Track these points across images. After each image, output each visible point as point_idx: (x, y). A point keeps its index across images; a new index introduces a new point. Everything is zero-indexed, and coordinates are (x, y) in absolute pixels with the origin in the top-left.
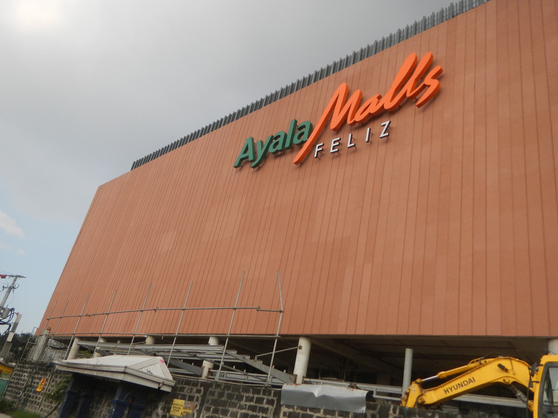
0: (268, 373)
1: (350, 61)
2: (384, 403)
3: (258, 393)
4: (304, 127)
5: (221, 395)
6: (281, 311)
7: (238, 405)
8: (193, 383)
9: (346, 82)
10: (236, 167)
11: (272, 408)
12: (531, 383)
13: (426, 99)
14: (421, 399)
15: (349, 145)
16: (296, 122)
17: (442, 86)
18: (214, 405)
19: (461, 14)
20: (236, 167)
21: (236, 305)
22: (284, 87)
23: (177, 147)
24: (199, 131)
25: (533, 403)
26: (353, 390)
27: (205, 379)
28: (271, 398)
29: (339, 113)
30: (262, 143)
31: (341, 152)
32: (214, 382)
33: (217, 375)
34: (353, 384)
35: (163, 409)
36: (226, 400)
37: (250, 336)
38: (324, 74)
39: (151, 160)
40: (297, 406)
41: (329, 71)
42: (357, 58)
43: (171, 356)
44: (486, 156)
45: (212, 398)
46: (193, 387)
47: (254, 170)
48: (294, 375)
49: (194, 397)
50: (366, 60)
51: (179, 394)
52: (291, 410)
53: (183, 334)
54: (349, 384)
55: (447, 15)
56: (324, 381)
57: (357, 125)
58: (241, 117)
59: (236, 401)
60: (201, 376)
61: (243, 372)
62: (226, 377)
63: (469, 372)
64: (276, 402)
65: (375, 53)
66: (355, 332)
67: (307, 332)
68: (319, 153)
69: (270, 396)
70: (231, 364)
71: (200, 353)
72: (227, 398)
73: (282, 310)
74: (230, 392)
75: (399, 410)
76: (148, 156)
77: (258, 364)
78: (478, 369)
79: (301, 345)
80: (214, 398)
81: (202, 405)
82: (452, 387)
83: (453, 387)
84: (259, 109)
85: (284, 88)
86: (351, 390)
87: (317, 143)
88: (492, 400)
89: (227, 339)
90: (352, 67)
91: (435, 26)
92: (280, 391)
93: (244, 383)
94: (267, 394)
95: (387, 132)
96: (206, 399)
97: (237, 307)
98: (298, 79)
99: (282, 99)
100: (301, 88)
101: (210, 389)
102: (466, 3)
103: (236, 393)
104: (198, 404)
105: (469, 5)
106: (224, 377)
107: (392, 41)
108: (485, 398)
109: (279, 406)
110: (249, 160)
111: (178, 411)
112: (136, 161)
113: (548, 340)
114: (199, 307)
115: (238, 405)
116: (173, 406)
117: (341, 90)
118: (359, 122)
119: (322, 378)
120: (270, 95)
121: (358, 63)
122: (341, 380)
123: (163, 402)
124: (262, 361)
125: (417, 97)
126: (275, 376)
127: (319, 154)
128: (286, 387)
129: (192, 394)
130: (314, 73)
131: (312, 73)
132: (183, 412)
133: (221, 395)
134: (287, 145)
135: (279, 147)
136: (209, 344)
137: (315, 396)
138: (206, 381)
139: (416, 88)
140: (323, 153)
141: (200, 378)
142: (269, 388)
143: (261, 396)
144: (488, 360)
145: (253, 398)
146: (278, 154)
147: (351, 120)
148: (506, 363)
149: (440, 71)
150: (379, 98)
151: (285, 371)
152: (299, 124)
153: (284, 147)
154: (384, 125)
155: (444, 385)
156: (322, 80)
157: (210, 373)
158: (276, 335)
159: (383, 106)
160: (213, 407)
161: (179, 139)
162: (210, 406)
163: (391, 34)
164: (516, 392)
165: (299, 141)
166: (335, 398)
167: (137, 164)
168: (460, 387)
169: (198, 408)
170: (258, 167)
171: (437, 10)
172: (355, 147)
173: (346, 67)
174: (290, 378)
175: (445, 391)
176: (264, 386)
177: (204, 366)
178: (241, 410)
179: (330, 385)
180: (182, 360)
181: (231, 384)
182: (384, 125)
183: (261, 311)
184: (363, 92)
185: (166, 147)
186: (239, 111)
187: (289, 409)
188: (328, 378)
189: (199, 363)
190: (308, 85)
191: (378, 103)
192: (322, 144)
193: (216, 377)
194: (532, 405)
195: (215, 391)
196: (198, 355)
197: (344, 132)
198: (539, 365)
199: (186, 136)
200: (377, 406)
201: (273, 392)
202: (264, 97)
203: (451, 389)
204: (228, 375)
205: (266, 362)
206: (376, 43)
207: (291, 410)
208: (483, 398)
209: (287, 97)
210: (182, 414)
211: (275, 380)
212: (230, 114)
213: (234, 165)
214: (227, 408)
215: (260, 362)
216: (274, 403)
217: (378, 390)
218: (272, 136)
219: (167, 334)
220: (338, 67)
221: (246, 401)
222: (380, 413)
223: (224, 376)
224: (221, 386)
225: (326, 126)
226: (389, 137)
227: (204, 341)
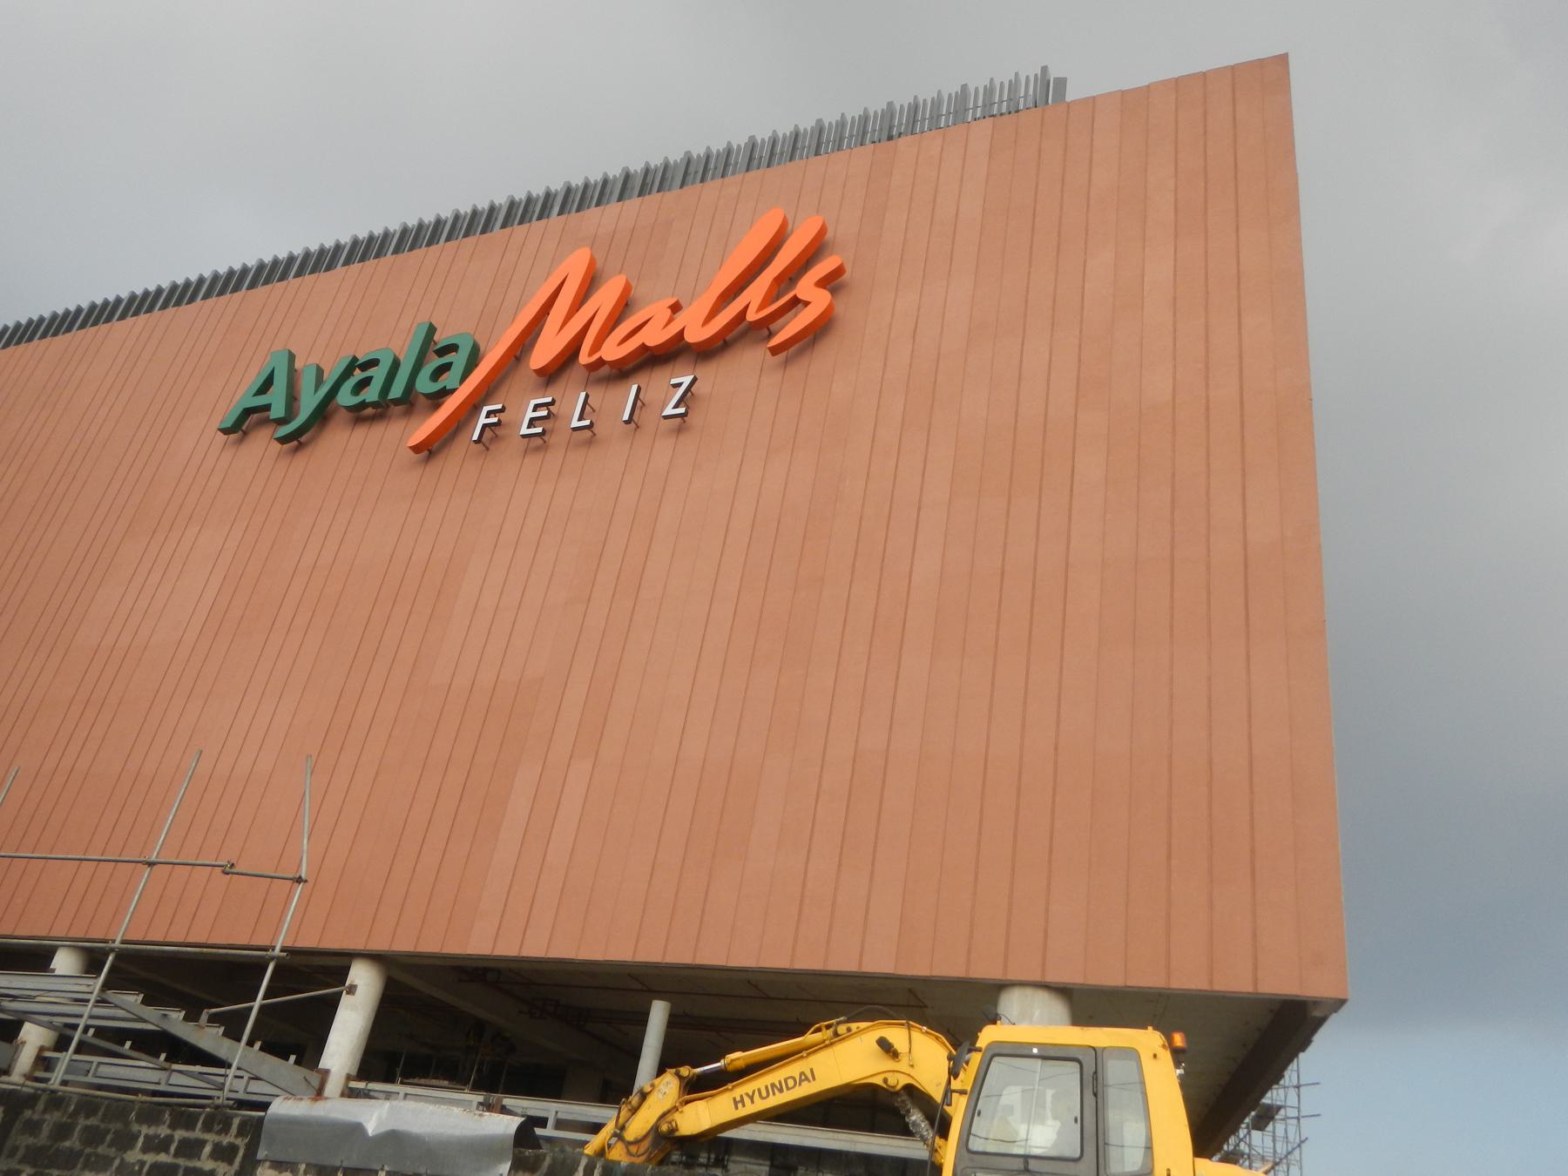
0: (230, 1060)
1: (611, 193)
2: (563, 1151)
3: (190, 1125)
4: (453, 348)
5: (62, 1131)
6: (300, 877)
7: (117, 1162)
9: (591, 249)
10: (226, 431)
12: (948, 1092)
14: (670, 1123)
15: (575, 423)
16: (432, 330)
17: (839, 309)
19: (910, 138)
20: (226, 431)
21: (158, 854)
25: (946, 1145)
26: (480, 1115)
27: (21, 1080)
28: (226, 1140)
29: (559, 331)
30: (320, 372)
31: (552, 439)
32: (44, 1090)
33: (57, 1070)
34: (494, 1097)
37: (189, 949)
38: (534, 212)
40: (307, 1165)
41: (549, 205)
42: (632, 189)
44: (919, 509)
45: (31, 1141)
47: (281, 449)
48: (319, 1071)
50: (653, 198)
54: (481, 1099)
55: (875, 131)
56: (409, 1090)
57: (605, 370)
58: (266, 282)
59: (112, 1152)
61: (155, 1060)
62: (95, 1076)
63: (804, 1054)
65: (681, 187)
67: (380, 944)
68: (487, 429)
69: (226, 1134)
70: (119, 1035)
71: (14, 998)
72: (80, 1141)
73: (303, 876)
74: (93, 1121)
75: (601, 1169)
77: (208, 1037)
78: (826, 1046)
79: (355, 984)
80: (35, 1141)
82: (754, 1092)
83: (757, 1092)
84: (325, 271)
86: (476, 1116)
87: (485, 402)
88: (851, 1141)
90: (613, 208)
91: (842, 150)
92: (261, 1120)
93: (155, 1093)
94: (217, 1128)
95: (683, 404)
97: (159, 860)
99: (401, 256)
100: (248, 289)
101: (28, 1113)
102: (900, 119)
103: (116, 1126)
105: (931, 117)
106: (87, 1075)
107: (755, 159)
108: (836, 1136)
110: (271, 417)
113: (1000, 987)
114: (33, 853)
115: (117, 1162)
117: (574, 267)
118: (612, 364)
121: (632, 200)
122: (460, 1087)
124: (223, 1028)
125: (773, 327)
126: (258, 1075)
127: (488, 433)
128: (281, 1107)
130: (620, 175)
131: (501, 200)
133: (62, 1131)
134: (396, 391)
135: (371, 394)
136: (53, 970)
137: (368, 1135)
138: (19, 1088)
139: (773, 302)
140: (499, 431)
142: (228, 1111)
143: (197, 1134)
144: (854, 1026)
145: (170, 1139)
146: (361, 415)
147: (590, 355)
148: (896, 1035)
149: (839, 271)
150: (676, 308)
151: (293, 1058)
152: (441, 339)
155: (734, 1087)
156: (526, 226)
157: (43, 1062)
158: (273, 950)
159: (682, 332)
161: (85, 305)
162: (18, 1167)
163: (729, 143)
164: (908, 1111)
165: (434, 387)
166: (427, 1139)
168: (774, 1094)
170: (296, 440)
171: (853, 112)
172: (592, 432)
173: (598, 205)
174: (306, 1080)
175: (736, 1103)
176: (212, 1103)
177: (24, 1039)
179: (416, 1101)
180: (91, 1031)
181: (102, 1097)
182: (679, 385)
183: (237, 874)
184: (633, 284)
186: (405, 231)
188: (423, 1081)
190: (484, 232)
191: (670, 321)
192: (499, 407)
193: (55, 1074)
194: (940, 1147)
195: (45, 1121)
197: (566, 384)
198: (973, 1049)
199: (111, 299)
200: (544, 1159)
201: (236, 1122)
203: (752, 1098)
204: (104, 1070)
205: (234, 1034)
206: (689, 161)
208: (830, 1135)
209: (416, 252)
211: (255, 1087)
213: (221, 422)
215: (216, 1029)
216: (235, 1156)
217: (560, 1116)
218: (355, 359)
220: (577, 199)
221: (145, 1150)
223: (89, 1071)
224: (68, 1105)
225: (518, 359)
226: (685, 418)
227: (35, 958)
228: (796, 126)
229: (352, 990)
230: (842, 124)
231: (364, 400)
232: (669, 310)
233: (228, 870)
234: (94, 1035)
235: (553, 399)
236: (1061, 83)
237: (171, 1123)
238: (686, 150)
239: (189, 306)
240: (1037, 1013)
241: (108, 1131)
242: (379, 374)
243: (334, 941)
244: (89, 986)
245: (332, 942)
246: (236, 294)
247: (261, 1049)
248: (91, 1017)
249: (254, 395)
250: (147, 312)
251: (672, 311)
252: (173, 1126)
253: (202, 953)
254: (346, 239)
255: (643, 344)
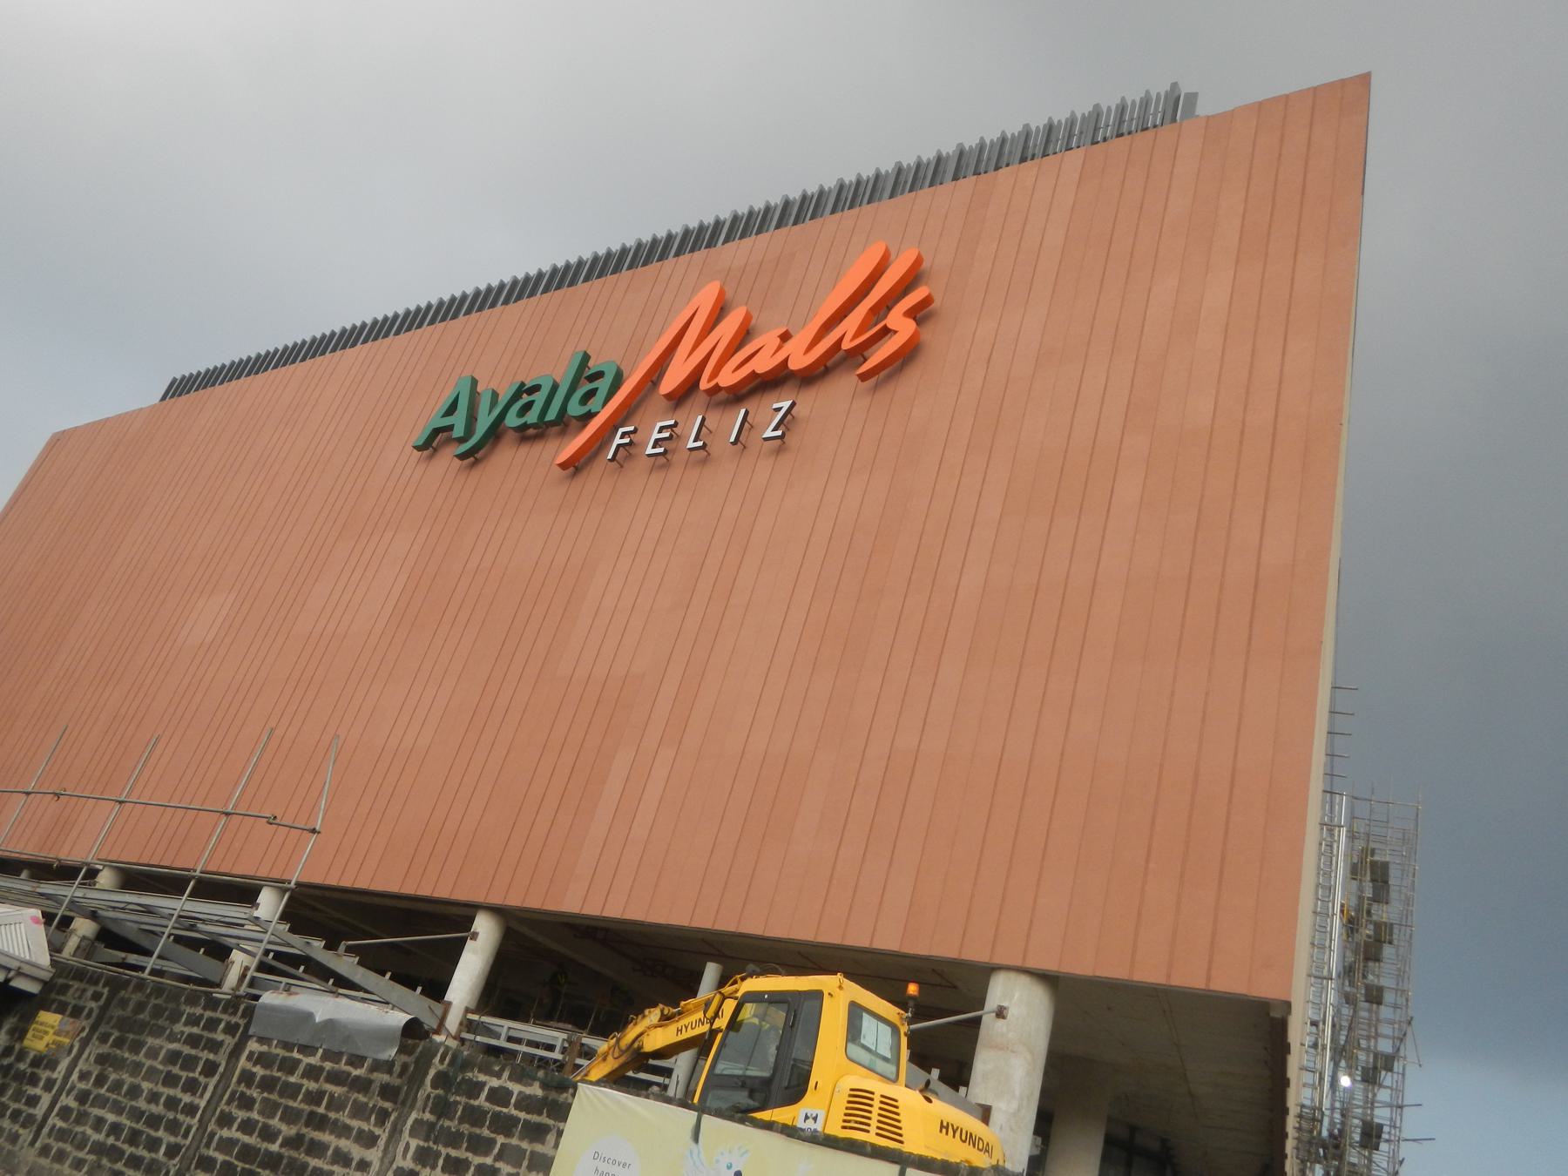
3: (214, 1009)
5: (140, 1007)
6: (314, 829)
8: (91, 978)
10: (418, 448)
11: (230, 1041)
13: (882, 362)
15: (691, 444)
16: (586, 358)
18: (120, 1030)
20: (418, 448)
22: (646, 238)
23: (242, 375)
24: (396, 316)
27: (67, 957)
28: (234, 1020)
30: (495, 395)
35: (11, 1032)
36: (148, 1019)
39: (273, 368)
40: (278, 1041)
43: (174, 928)
46: (87, 986)
49: (82, 1009)
51: (54, 1001)
52: (264, 1048)
53: (140, 865)
57: (722, 395)
60: (219, 985)
61: (324, 984)
64: (241, 1029)
66: (871, 942)
67: (495, 899)
68: (621, 448)
73: (317, 828)
74: (159, 1001)
76: (241, 361)
80: (123, 1013)
81: (94, 1028)
85: (614, 250)
89: (192, 883)
94: (230, 1011)
96: (108, 1015)
98: (640, 239)
100: (542, 294)
102: (1036, 139)
103: (171, 1006)
104: (87, 1024)
109: (245, 1037)
111: (41, 1038)
112: (179, 377)
116: (34, 1026)
117: (705, 300)
118: (730, 389)
119: (537, 1022)
120: (648, 241)
123: (14, 1017)
124: (357, 959)
127: (622, 451)
129: (81, 1003)
132: (51, 1042)
133: (140, 1007)
134: (551, 415)
135: (532, 417)
140: (632, 451)
141: (217, 990)
143: (218, 1015)
146: (527, 434)
149: (927, 301)
152: (593, 366)
153: (544, 418)
154: (779, 409)
159: (786, 360)
160: (116, 1034)
165: (583, 410)
167: (180, 387)
169: (84, 1034)
170: (472, 456)
174: (430, 1008)
178: (170, 1042)
180: (271, 955)
181: (168, 984)
182: (779, 409)
184: (755, 315)
185: (268, 353)
186: (736, 219)
187: (261, 1045)
189: (220, 951)
190: (795, 223)
192: (632, 428)
196: (201, 926)
199: (358, 324)
201: (242, 1007)
202: (679, 231)
206: (899, 170)
207: (264, 1048)
210: (47, 1045)
212: (502, 281)
214: (142, 1038)
215: (353, 959)
218: (523, 384)
219: (135, 864)
221: (186, 1024)
222: (417, 1062)
227: (245, 893)
228: (1050, 118)
229: (475, 936)
230: (1072, 122)
231: (526, 422)
232: (779, 339)
233: (272, 821)
234: (273, 958)
235: (676, 422)
236: (1192, 98)
237: (204, 1006)
238: (1025, 123)
239: (352, 349)
240: (1017, 995)
241: (166, 1009)
242: (539, 398)
243: (463, 893)
244: (245, 913)
245: (461, 895)
246: (532, 299)
247: (390, 979)
248: (269, 943)
249: (443, 416)
250: (341, 349)
251: (781, 339)
252: (205, 1008)
253: (246, 883)
254: (677, 229)
255: (754, 371)
